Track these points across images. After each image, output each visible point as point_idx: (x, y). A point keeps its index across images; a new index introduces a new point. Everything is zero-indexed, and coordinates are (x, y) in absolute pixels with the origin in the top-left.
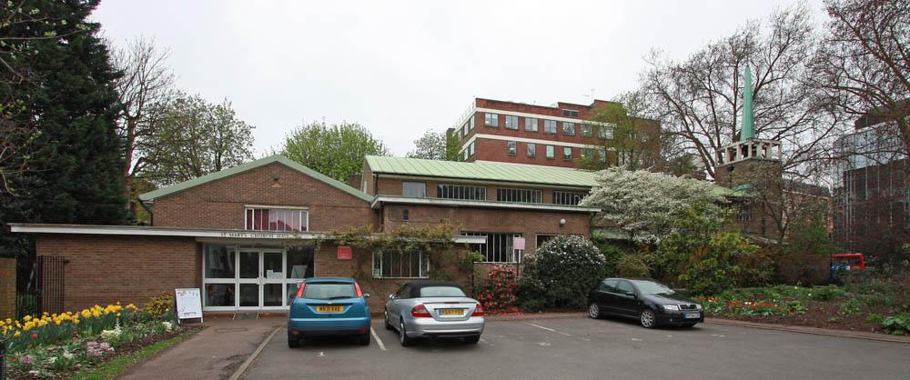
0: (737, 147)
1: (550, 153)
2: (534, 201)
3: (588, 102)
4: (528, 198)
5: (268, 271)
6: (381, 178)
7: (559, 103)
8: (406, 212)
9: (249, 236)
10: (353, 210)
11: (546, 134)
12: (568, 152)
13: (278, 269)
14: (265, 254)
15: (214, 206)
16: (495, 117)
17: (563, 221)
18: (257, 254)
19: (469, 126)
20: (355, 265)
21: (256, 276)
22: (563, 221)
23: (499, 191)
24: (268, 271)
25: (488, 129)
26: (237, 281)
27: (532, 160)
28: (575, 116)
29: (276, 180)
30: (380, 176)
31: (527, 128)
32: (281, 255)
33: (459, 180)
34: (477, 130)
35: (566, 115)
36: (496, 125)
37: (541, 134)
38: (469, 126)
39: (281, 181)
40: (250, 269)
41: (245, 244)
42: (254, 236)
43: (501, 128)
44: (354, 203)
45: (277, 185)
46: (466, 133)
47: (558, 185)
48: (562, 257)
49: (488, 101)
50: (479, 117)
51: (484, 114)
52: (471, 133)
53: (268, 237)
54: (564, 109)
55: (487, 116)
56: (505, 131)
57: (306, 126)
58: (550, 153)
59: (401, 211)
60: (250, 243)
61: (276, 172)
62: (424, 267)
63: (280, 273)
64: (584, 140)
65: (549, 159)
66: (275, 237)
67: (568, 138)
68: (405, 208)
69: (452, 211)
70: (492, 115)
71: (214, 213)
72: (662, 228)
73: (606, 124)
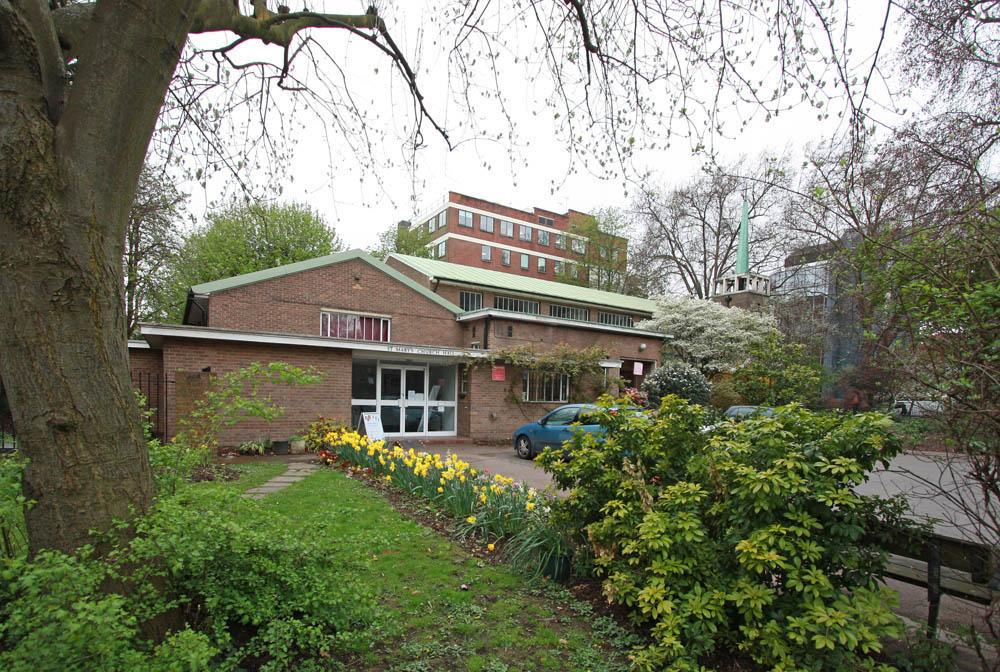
0: (736, 279)
1: (486, 255)
2: (577, 318)
3: (562, 211)
4: (515, 308)
5: (410, 392)
6: (444, 285)
7: (536, 209)
8: (510, 328)
9: (384, 348)
10: (438, 321)
11: (521, 241)
12: (542, 263)
13: (420, 390)
14: (408, 372)
15: (285, 307)
16: (470, 216)
17: (644, 346)
18: (399, 371)
19: (437, 222)
20: (508, 388)
21: (397, 396)
22: (644, 346)
23: (462, 294)
24: (410, 392)
25: (462, 229)
26: (379, 402)
27: (506, 268)
28: (550, 224)
29: (357, 279)
30: (441, 282)
31: (503, 232)
32: (422, 373)
33: (474, 287)
34: (447, 229)
35: (542, 222)
36: (468, 222)
37: (514, 240)
38: (437, 222)
39: (361, 281)
40: (391, 390)
41: (386, 358)
42: (420, 352)
43: (475, 230)
44: (439, 313)
45: (357, 287)
46: (432, 229)
47: (606, 305)
48: (683, 385)
49: (463, 196)
50: (452, 213)
51: (457, 211)
52: (439, 231)
53: (435, 353)
54: (541, 216)
55: (461, 214)
56: (458, 229)
57: (291, 205)
58: (486, 255)
59: (505, 327)
60: (415, 359)
61: (357, 270)
62: (564, 391)
63: (421, 394)
64: (558, 252)
65: (523, 269)
66: (441, 353)
67: (543, 248)
68: (510, 324)
69: (551, 330)
70: (466, 213)
71: (285, 316)
72: (729, 356)
73: (580, 238)
